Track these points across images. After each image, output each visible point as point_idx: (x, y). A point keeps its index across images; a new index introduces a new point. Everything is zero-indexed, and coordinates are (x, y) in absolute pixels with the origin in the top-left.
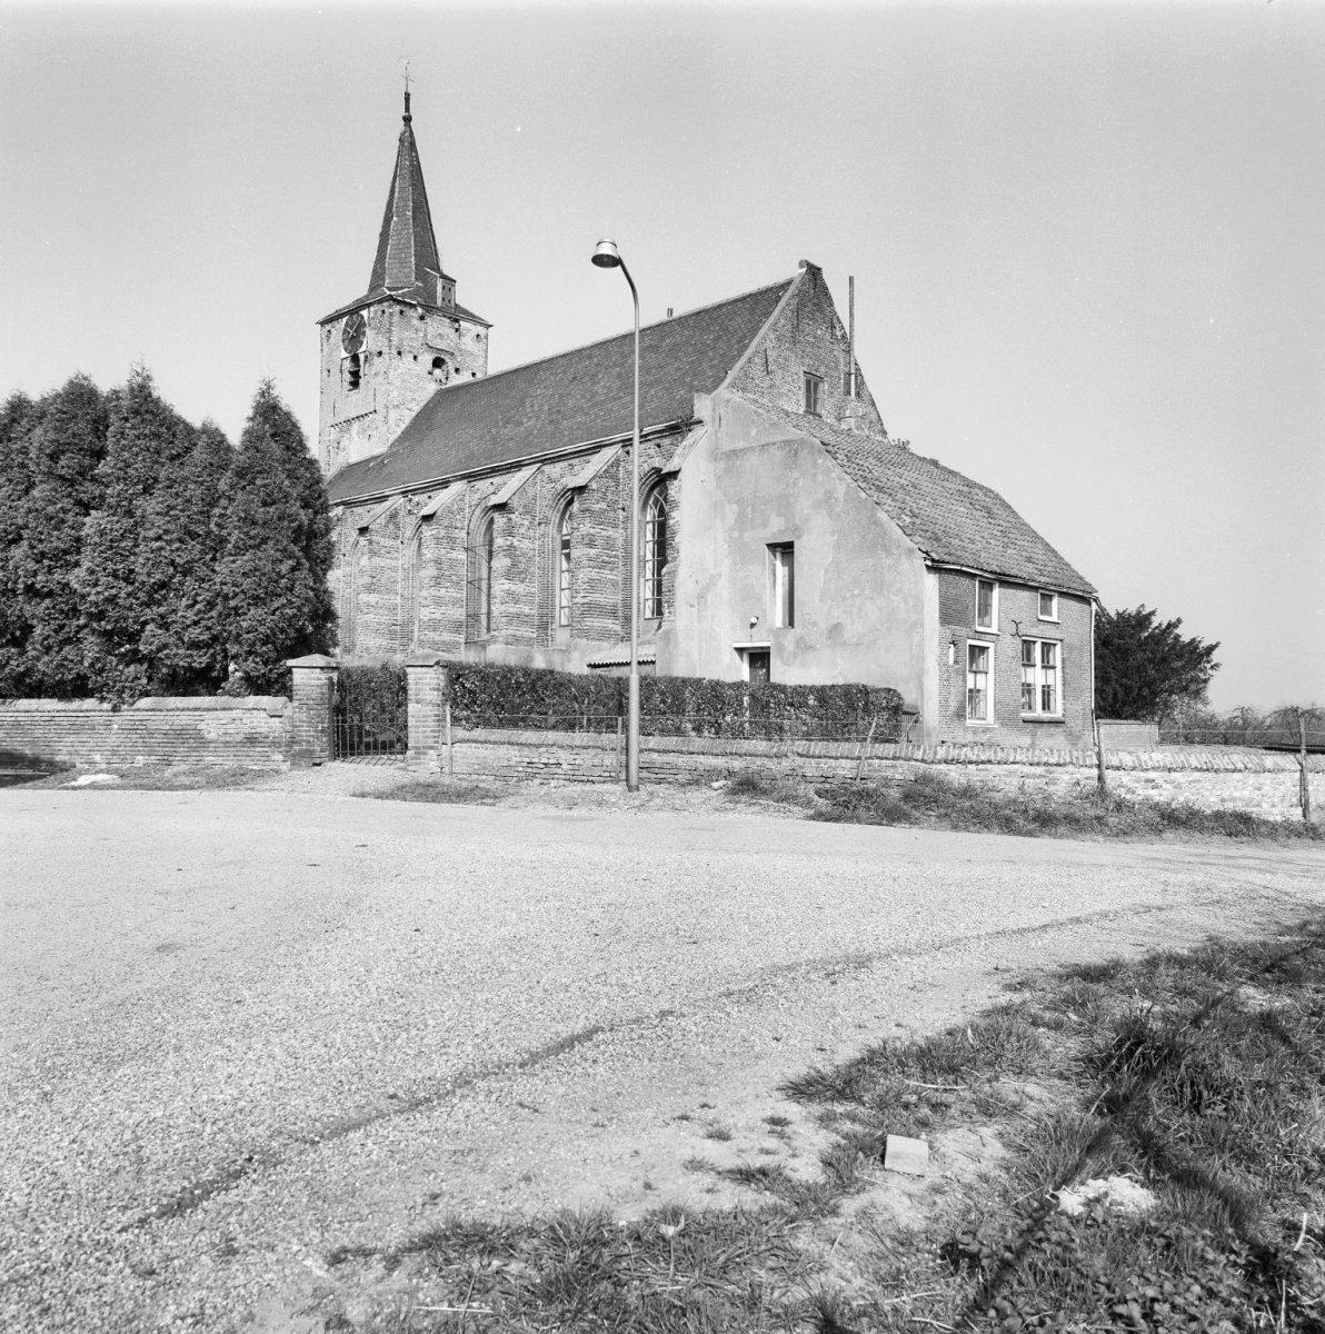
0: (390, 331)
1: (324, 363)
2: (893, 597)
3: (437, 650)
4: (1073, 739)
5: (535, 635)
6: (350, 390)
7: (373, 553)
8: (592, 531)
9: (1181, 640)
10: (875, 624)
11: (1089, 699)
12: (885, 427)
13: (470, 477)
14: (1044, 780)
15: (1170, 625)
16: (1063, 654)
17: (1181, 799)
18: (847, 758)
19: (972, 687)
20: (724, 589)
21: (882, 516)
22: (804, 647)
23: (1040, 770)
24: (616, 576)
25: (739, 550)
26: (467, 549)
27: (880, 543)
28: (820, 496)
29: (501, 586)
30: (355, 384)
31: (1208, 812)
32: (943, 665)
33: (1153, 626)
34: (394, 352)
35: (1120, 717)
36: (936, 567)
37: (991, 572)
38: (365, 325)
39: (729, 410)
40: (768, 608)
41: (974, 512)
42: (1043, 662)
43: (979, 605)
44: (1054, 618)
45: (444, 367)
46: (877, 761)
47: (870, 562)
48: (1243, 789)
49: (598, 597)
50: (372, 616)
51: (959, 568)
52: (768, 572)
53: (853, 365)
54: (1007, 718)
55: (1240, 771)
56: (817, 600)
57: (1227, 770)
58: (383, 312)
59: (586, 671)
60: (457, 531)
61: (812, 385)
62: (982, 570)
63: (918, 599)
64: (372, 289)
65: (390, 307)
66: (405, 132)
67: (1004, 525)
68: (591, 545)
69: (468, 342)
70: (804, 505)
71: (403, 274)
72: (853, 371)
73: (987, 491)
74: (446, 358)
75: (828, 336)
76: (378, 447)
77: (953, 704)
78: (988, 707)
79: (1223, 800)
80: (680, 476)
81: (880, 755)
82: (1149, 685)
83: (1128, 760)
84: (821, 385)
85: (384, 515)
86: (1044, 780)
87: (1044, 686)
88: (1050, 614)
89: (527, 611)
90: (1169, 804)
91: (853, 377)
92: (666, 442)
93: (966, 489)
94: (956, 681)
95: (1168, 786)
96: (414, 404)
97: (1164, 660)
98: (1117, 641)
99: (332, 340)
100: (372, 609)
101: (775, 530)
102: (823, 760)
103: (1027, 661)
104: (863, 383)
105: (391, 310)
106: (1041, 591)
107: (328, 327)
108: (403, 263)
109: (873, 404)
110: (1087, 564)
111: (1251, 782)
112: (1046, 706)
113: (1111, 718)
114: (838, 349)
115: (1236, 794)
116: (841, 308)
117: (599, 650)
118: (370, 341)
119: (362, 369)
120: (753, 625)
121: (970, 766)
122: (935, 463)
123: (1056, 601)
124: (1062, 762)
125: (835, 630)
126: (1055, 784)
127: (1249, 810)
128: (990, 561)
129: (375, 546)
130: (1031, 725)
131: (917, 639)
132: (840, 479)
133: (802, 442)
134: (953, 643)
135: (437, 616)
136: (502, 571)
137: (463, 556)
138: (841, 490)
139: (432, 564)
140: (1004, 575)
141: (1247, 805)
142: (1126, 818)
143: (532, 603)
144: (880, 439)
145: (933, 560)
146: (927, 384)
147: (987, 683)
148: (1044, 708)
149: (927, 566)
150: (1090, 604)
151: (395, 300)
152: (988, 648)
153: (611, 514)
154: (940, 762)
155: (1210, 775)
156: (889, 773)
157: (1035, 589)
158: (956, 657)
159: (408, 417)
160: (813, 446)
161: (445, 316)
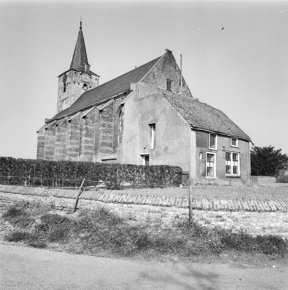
0: (72, 77)
2: (182, 139)
4: (244, 182)
5: (94, 152)
6: (64, 92)
8: (104, 122)
9: (281, 154)
10: (181, 149)
11: (249, 170)
12: (192, 95)
14: (160, 214)
15: (278, 151)
16: (240, 157)
17: (238, 228)
18: (71, 198)
19: (209, 166)
20: (138, 137)
21: (179, 114)
22: (158, 154)
23: (158, 208)
24: (112, 135)
25: (141, 125)
26: (80, 130)
27: (178, 122)
28: (162, 109)
29: (84, 138)
31: (254, 236)
32: (197, 159)
33: (273, 151)
34: (73, 82)
35: (264, 175)
36: (194, 129)
37: (214, 131)
39: (141, 87)
40: (149, 143)
41: (213, 116)
42: (233, 159)
43: (211, 141)
44: (237, 146)
45: (87, 86)
46: (84, 200)
47: (176, 128)
48: (276, 222)
49: (106, 141)
50: (58, 147)
51: (203, 130)
52: (149, 133)
53: (182, 78)
54: (220, 176)
55: (274, 211)
56: (161, 140)
57: (266, 211)
58: (71, 73)
59: (101, 162)
61: (169, 83)
62: (211, 130)
63: (189, 139)
64: (70, 68)
65: (72, 71)
66: (80, 31)
67: (223, 119)
68: (104, 126)
70: (158, 112)
71: (78, 64)
72: (182, 79)
73: (219, 111)
75: (174, 70)
77: (201, 172)
78: (214, 173)
79: (264, 228)
80: (124, 105)
81: (84, 197)
82: (273, 167)
83: (206, 204)
84: (172, 83)
85: (62, 122)
86: (160, 214)
87: (233, 166)
88: (235, 145)
90: (231, 231)
91: (182, 81)
92: (123, 97)
93: (212, 110)
94: (202, 165)
95: (230, 220)
96: (78, 95)
97: (276, 160)
98: (263, 155)
99: (61, 81)
101: (151, 120)
102: (62, 199)
103: (228, 158)
104: (185, 83)
105: (72, 72)
106: (232, 138)
107: (60, 78)
108: (77, 62)
109: (188, 89)
110: (247, 129)
111: (281, 217)
112: (235, 172)
113: (262, 175)
114: (177, 74)
115: (272, 225)
116: (178, 62)
117: (105, 156)
118: (68, 80)
120: (145, 148)
121: (124, 205)
122: (205, 104)
123: (237, 141)
124: (169, 205)
125: (166, 149)
126: (166, 217)
127: (280, 234)
128: (215, 128)
129: (60, 130)
130: (229, 178)
131: (188, 151)
132: (168, 104)
133: (158, 94)
134: (201, 152)
135: (71, 147)
136: (84, 134)
137: (79, 131)
138: (168, 107)
140: (219, 132)
141: (279, 231)
142: (200, 242)
143: (93, 143)
144: (191, 98)
145: (193, 127)
146: (205, 82)
147: (213, 165)
148: (234, 173)
149: (191, 129)
150: (249, 142)
151: (74, 70)
152: (214, 155)
153: (110, 118)
154: (110, 202)
155: (256, 214)
156: (88, 207)
157: (230, 137)
158: (202, 157)
159: (76, 98)
160: (161, 95)
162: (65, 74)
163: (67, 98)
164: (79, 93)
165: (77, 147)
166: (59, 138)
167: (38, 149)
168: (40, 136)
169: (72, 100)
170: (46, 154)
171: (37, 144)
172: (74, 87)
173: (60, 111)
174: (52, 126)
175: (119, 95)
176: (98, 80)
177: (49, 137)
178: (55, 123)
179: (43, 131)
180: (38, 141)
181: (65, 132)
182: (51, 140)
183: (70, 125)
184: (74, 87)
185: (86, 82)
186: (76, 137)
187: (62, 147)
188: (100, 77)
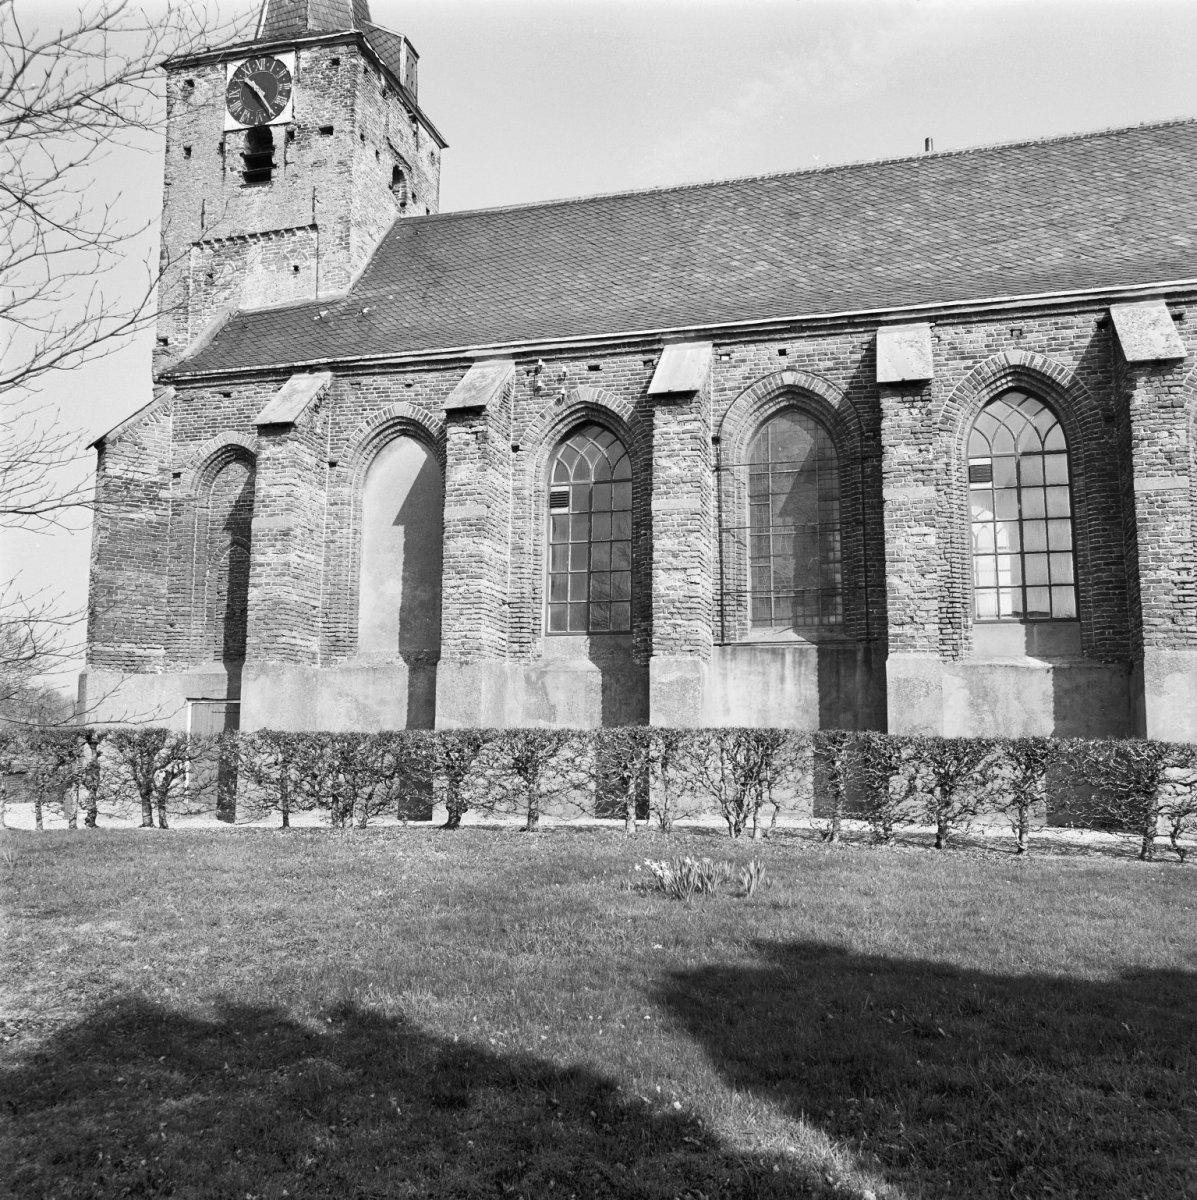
6: (242, 186)
58: (336, 62)
105: (354, 61)
118: (296, 107)
139: (687, 487)
161: (404, 104)
163: (299, 233)
179: (146, 443)
188: (445, 146)
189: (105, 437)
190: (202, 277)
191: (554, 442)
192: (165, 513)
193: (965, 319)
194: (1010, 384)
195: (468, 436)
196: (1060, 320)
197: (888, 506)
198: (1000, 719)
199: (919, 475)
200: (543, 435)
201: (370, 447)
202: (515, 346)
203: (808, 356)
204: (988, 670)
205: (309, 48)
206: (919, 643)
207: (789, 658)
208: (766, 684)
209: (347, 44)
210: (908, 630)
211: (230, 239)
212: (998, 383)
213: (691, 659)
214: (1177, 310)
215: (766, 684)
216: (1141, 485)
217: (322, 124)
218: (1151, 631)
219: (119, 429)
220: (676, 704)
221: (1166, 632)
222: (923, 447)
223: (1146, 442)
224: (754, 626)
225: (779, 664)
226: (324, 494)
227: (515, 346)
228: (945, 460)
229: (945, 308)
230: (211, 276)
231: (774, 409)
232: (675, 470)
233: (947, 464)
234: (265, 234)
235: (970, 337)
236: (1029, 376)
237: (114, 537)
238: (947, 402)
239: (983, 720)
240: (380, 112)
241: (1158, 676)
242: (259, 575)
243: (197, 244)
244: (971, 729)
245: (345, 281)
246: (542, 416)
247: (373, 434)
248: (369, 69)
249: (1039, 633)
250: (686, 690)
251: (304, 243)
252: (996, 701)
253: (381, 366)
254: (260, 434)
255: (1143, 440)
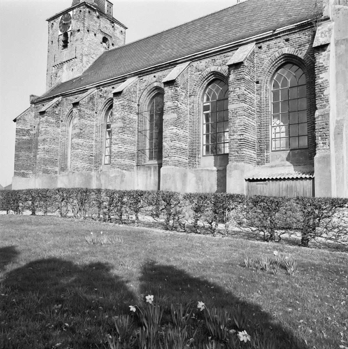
0: (84, 19)
1: (50, 39)
3: (123, 169)
5: (187, 161)
6: (62, 49)
7: (81, 117)
13: (140, 74)
26: (138, 114)
30: (65, 46)
38: (71, 18)
58: (81, 11)
60: (133, 103)
65: (84, 8)
69: (117, 33)
74: (109, 38)
76: (77, 74)
89: (184, 146)
100: (80, 147)
105: (84, 10)
107: (52, 22)
118: (74, 25)
119: (69, 39)
129: (82, 113)
135: (123, 150)
137: (136, 117)
139: (120, 120)
159: (92, 61)
161: (107, 19)
162: (64, 14)
163: (73, 60)
164: (95, 52)
165: (133, 151)
166: (82, 131)
167: (17, 153)
168: (21, 128)
169: (85, 64)
170: (44, 164)
171: (15, 143)
172: (88, 39)
173: (56, 82)
174: (54, 107)
175: (276, 32)
176: (124, 34)
177: (49, 129)
178: (59, 103)
179: (27, 119)
180: (17, 138)
181: (93, 119)
182: (53, 135)
183: (118, 103)
184: (88, 39)
185: (107, 34)
186: (131, 128)
187: (87, 149)
188: (127, 28)
189: (16, 119)
190: (55, 75)
191: (106, 110)
192: (32, 137)
193: (199, 58)
194: (214, 78)
195: (77, 111)
196: (226, 54)
197: (164, 121)
198: (204, 187)
199: (173, 110)
200: (102, 108)
201: (70, 116)
202: (98, 83)
203: (160, 77)
204: (201, 171)
205: (75, 9)
206: (170, 163)
207: (152, 169)
208: (147, 177)
209: (83, 6)
210: (167, 159)
211: (60, 64)
212: (210, 78)
213: (118, 170)
214: (259, 45)
215: (147, 177)
216: (231, 107)
217: (78, 29)
218: (231, 156)
219: (20, 116)
220: (114, 183)
221: (235, 156)
222: (174, 101)
223: (233, 92)
224: (150, 160)
225: (150, 170)
226: (60, 129)
227: (98, 83)
228: (192, 105)
229: (194, 56)
230: (56, 74)
231: (154, 94)
232: (117, 115)
233: (193, 106)
234: (66, 61)
235: (201, 64)
236: (218, 74)
237: (19, 144)
238: (194, 86)
239: (199, 187)
240: (96, 22)
241: (230, 171)
242: (39, 151)
243: (53, 66)
244: (196, 190)
245: (81, 71)
246: (102, 103)
247: (70, 112)
248: (91, 11)
249: (219, 159)
250: (116, 179)
251: (74, 62)
252: (203, 181)
253: (71, 93)
254: (40, 115)
255: (232, 92)
